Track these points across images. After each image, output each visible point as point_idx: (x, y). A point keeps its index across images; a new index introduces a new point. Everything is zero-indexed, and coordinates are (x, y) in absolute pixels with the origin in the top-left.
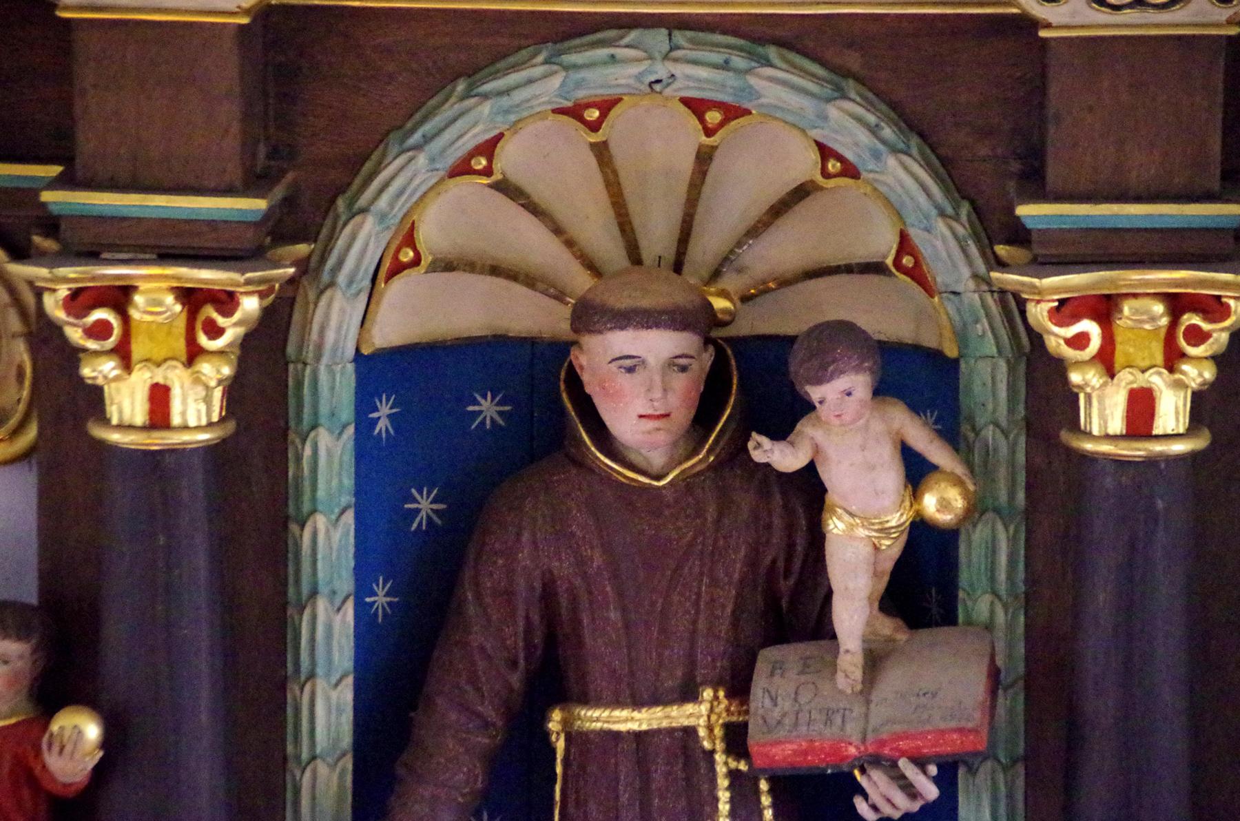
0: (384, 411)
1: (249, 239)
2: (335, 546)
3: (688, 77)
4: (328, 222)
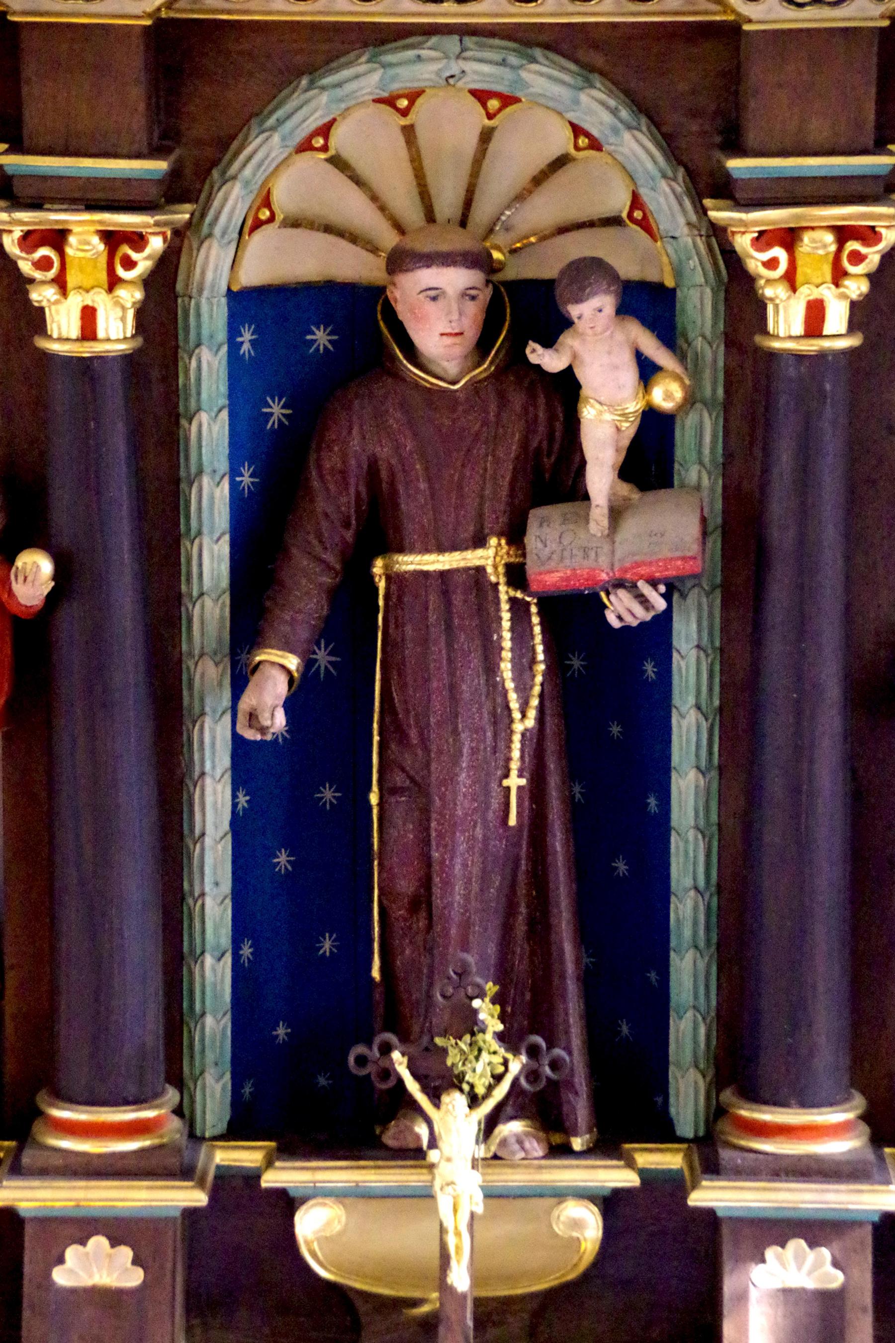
0: (247, 336)
1: (153, 193)
2: (215, 436)
3: (475, 72)
4: (207, 187)
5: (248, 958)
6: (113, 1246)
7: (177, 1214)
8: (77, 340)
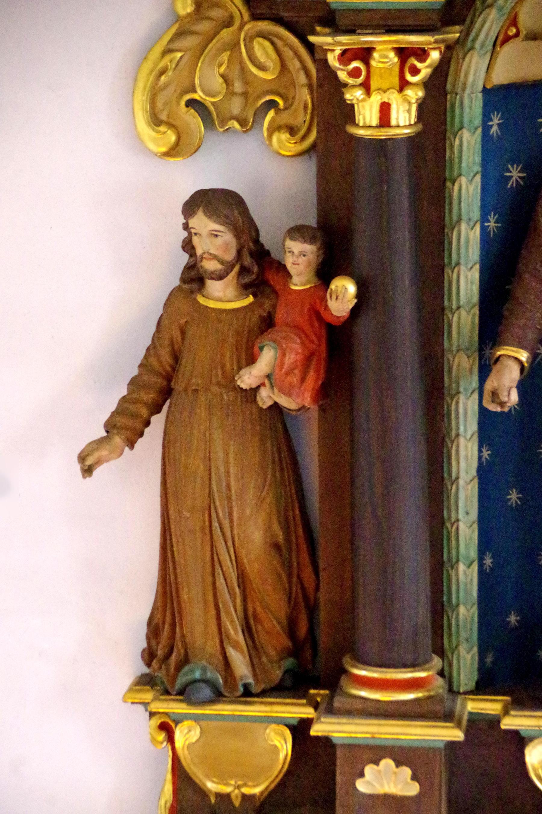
0: (496, 120)
2: (471, 194)
5: (489, 566)
6: (397, 766)
7: (442, 745)
8: (376, 127)
